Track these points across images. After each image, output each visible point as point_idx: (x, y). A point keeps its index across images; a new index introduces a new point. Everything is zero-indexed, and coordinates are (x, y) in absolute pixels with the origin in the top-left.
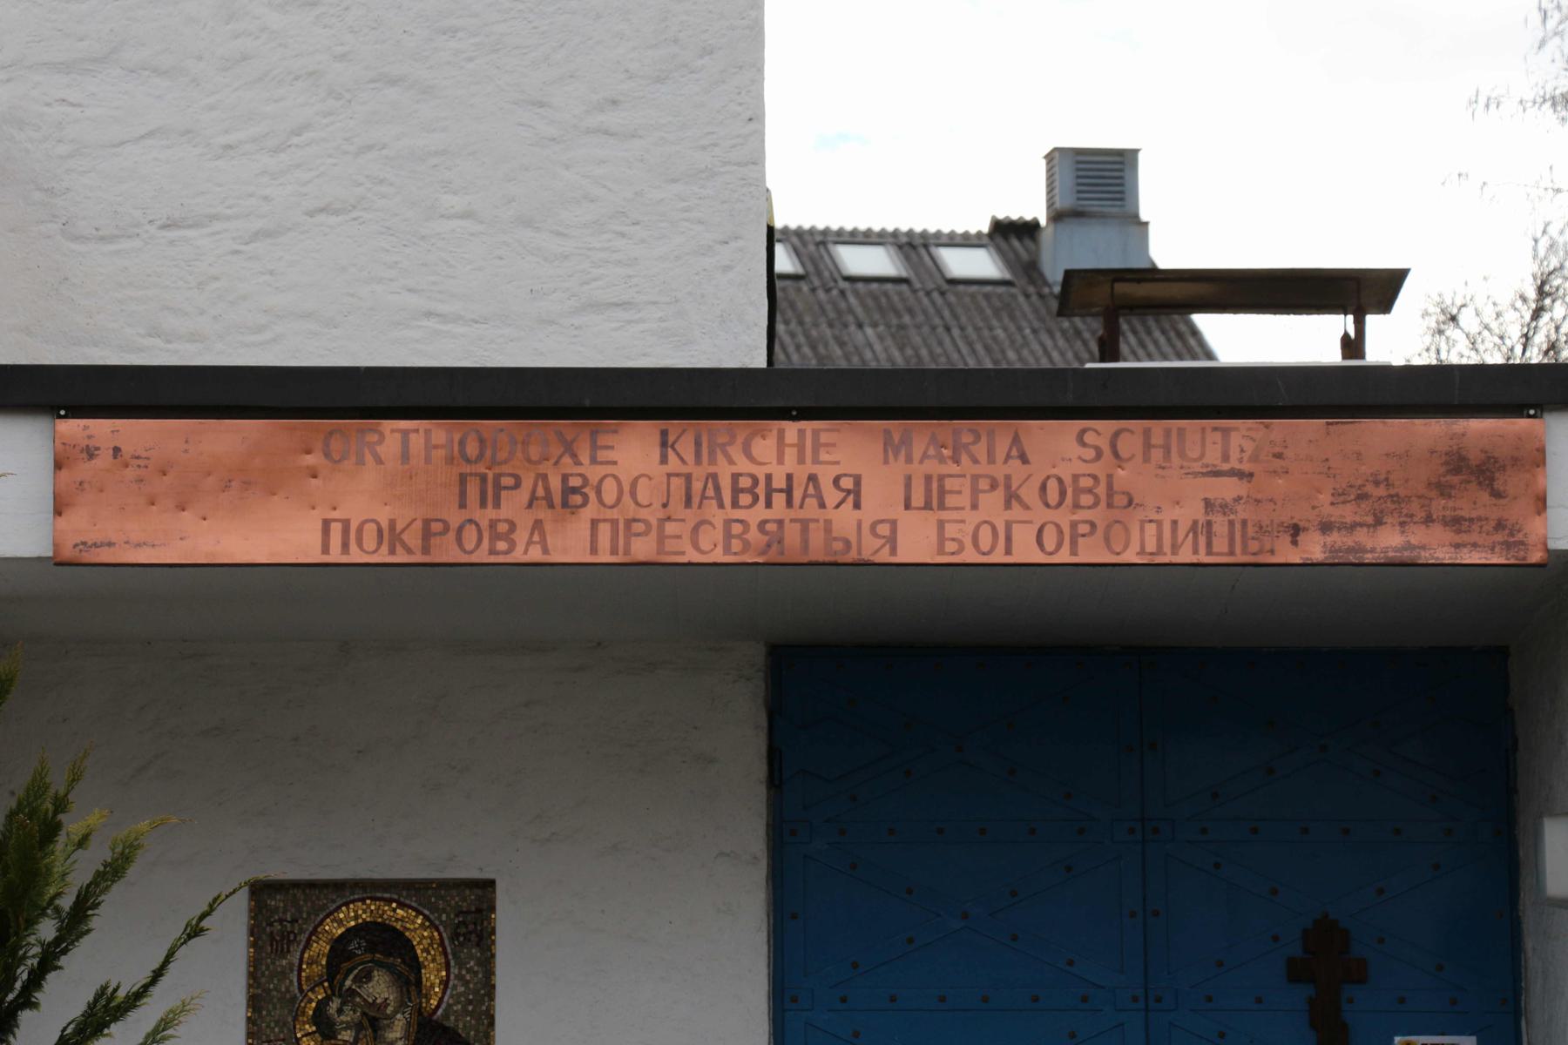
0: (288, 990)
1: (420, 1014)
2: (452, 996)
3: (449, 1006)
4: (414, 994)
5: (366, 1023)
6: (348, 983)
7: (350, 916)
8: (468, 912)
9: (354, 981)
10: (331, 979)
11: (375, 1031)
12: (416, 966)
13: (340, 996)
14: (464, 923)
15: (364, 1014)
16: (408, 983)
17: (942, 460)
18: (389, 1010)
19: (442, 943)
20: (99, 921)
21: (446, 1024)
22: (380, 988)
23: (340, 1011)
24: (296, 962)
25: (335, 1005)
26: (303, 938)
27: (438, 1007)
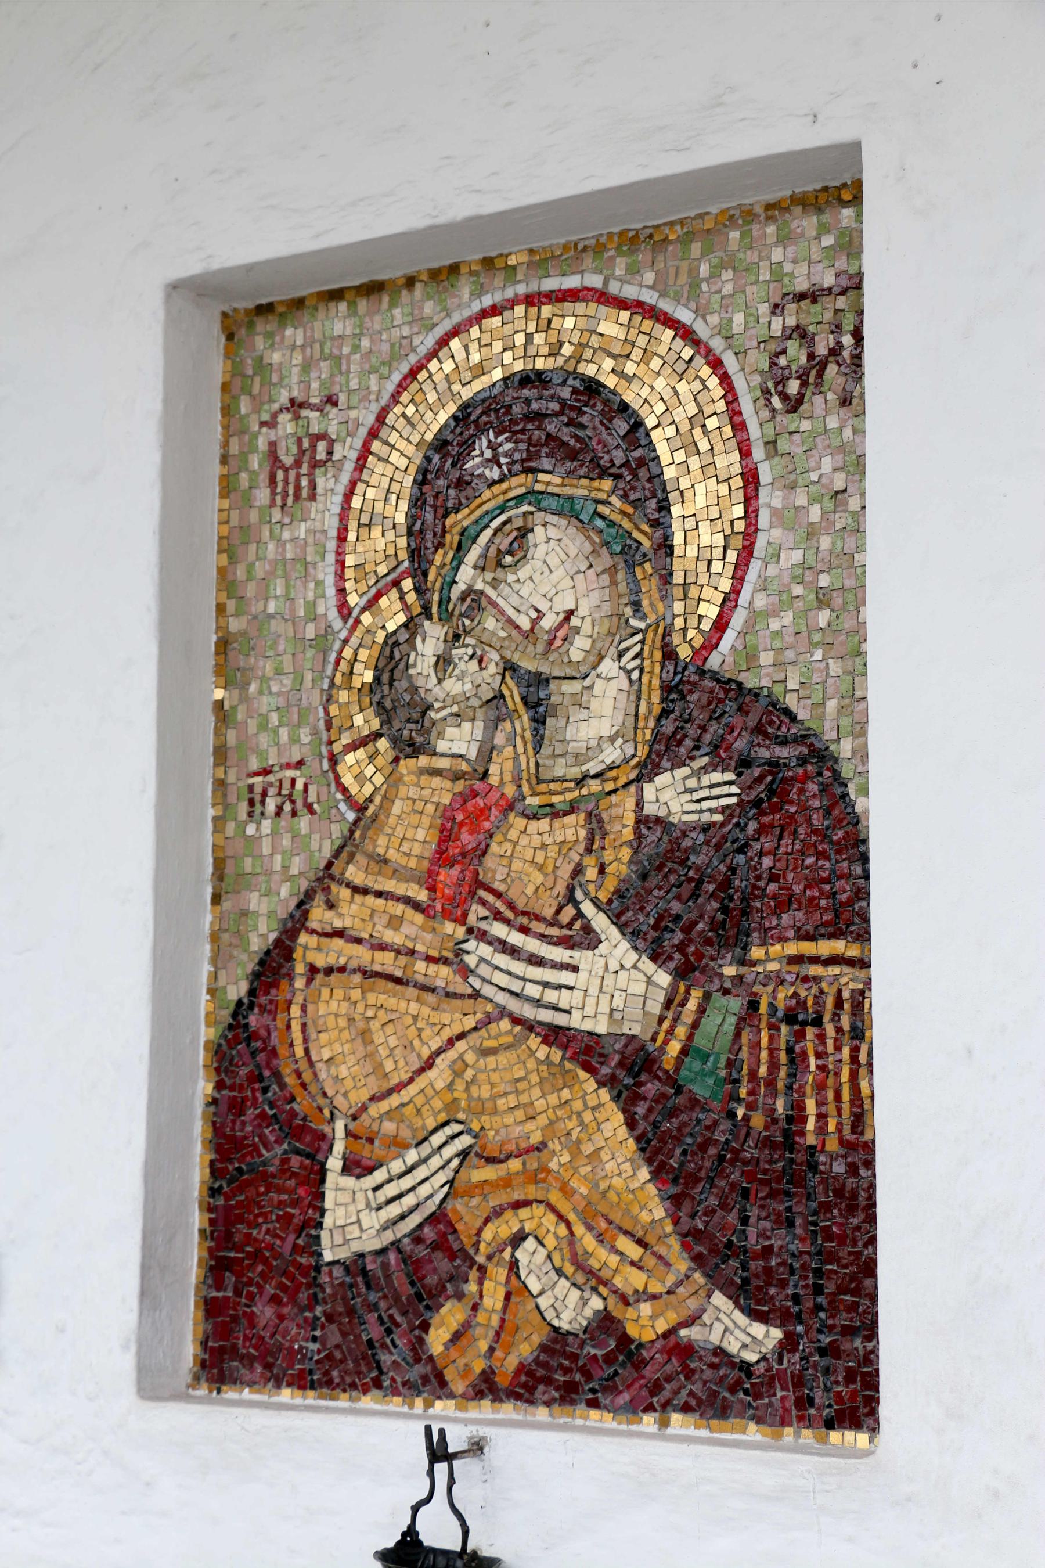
0: (311, 606)
1: (669, 654)
2: (763, 586)
3: (754, 616)
4: (650, 587)
5: (514, 694)
6: (466, 575)
7: (489, 356)
8: (811, 296)
9: (480, 568)
10: (419, 573)
11: (539, 721)
12: (654, 499)
13: (446, 616)
14: (800, 332)
15: (510, 668)
16: (629, 555)
17: (307, 1348)
18: (579, 648)
19: (734, 414)
20: (867, 332)
21: (750, 681)
22: (555, 577)
23: (443, 663)
24: (332, 524)
25: (431, 640)
26: (347, 451)
27: (721, 625)
